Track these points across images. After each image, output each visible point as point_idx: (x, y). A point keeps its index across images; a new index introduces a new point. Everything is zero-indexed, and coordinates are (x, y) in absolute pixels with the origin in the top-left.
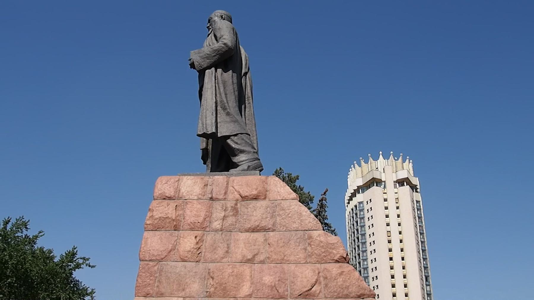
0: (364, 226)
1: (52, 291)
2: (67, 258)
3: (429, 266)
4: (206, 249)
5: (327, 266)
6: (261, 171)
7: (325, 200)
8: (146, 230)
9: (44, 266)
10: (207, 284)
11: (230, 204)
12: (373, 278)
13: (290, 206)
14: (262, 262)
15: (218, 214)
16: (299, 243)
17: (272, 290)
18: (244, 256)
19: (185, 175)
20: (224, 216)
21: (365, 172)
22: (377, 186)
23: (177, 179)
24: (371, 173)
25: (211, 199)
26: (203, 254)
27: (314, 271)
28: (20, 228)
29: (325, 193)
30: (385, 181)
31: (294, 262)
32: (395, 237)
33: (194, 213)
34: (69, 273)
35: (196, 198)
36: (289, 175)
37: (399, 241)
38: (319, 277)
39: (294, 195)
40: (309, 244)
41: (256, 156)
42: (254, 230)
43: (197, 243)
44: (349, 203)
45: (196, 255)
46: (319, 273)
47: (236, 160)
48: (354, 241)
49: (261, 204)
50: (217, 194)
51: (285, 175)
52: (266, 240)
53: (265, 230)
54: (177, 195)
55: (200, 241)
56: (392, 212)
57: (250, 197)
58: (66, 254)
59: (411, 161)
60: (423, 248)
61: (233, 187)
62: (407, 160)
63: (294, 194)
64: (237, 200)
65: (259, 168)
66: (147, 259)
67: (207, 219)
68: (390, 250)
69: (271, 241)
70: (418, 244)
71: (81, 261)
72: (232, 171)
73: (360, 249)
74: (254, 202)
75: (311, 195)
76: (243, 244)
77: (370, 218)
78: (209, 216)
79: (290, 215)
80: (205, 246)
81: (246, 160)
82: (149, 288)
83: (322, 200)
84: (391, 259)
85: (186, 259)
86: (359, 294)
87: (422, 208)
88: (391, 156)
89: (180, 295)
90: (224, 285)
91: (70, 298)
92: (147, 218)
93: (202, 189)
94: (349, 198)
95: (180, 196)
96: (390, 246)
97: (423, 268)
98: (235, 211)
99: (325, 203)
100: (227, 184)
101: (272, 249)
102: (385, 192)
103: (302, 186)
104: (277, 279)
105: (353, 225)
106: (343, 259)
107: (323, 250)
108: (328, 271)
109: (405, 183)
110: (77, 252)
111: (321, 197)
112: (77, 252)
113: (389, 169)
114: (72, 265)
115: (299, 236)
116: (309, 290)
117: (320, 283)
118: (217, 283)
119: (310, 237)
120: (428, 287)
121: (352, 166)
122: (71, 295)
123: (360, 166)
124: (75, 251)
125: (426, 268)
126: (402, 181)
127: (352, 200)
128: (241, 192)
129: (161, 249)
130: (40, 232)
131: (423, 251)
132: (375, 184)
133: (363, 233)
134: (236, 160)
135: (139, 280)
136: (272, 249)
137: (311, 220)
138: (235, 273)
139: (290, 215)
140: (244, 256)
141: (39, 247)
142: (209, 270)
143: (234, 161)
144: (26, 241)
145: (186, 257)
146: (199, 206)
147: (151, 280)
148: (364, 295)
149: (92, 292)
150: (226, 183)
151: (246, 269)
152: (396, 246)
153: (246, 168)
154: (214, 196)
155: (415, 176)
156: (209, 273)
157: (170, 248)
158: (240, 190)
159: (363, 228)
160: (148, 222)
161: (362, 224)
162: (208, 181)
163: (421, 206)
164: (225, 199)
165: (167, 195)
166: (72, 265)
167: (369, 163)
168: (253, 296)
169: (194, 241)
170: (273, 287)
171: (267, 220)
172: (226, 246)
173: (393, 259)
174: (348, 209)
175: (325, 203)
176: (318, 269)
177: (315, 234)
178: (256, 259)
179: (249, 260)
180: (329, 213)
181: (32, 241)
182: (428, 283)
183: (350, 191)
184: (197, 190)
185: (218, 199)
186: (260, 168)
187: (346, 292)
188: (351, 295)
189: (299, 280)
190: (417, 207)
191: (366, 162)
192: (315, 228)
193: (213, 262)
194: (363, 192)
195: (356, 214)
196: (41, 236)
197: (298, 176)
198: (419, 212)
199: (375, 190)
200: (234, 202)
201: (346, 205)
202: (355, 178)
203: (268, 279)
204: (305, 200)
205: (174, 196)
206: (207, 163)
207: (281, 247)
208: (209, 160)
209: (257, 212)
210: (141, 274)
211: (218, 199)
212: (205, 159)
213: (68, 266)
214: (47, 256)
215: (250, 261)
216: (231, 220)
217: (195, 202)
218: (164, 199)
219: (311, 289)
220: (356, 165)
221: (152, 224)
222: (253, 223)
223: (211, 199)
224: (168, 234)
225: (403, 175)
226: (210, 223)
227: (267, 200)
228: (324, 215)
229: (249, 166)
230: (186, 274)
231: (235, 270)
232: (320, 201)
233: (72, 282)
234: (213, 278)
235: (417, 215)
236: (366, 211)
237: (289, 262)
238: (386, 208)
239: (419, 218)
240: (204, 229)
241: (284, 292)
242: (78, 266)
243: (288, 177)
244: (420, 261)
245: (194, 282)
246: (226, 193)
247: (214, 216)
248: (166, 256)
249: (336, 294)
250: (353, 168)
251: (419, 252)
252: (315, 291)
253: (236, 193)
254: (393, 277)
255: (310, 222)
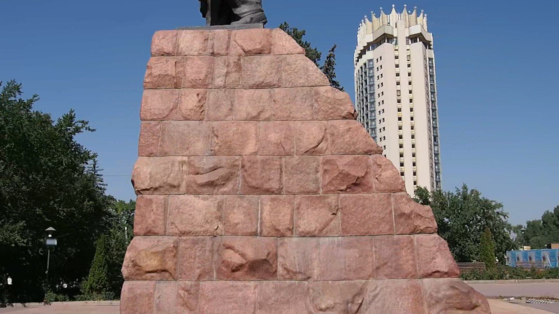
0: (373, 85)
1: (53, 155)
2: (64, 122)
3: (438, 126)
4: (209, 107)
5: (335, 122)
6: (264, 23)
7: (333, 57)
8: (145, 88)
9: (41, 130)
10: (211, 142)
11: (233, 59)
12: (380, 112)
13: (296, 61)
14: (268, 119)
15: (220, 69)
16: (306, 99)
17: (278, 148)
18: (248, 114)
19: (183, 29)
20: (227, 72)
21: (376, 27)
22: (388, 42)
23: (175, 34)
24: (382, 29)
25: (213, 54)
26: (206, 111)
27: (321, 129)
28: (13, 92)
29: (333, 50)
30: (396, 37)
31: (301, 119)
32: (405, 97)
33: (194, 69)
34: (69, 137)
35: (196, 53)
36: (295, 30)
37: (413, 183)
38: (325, 133)
39: (300, 49)
40: (316, 100)
41: (260, 7)
42: (259, 86)
43: (200, 101)
44: (358, 61)
45: (199, 114)
46: (326, 130)
47: (237, 11)
48: (363, 100)
49: (265, 58)
50: (218, 49)
51: (290, 31)
52: (271, 97)
53: (270, 86)
54: (176, 51)
55: (202, 99)
56: (404, 79)
57: (254, 52)
58: (64, 117)
59: (426, 15)
60: (434, 108)
61: (235, 41)
62: (422, 14)
63: (301, 47)
64: (240, 55)
65: (263, 20)
66: (148, 118)
67: (209, 76)
68: (399, 110)
69: (277, 97)
70: (428, 103)
71: (80, 125)
72: (234, 24)
73: (369, 109)
74: (258, 57)
75: (318, 52)
76: (247, 101)
77: (382, 129)
78: (210, 74)
79: (296, 71)
80: (208, 104)
81: (249, 12)
82: (152, 148)
83: (330, 57)
84: (400, 119)
85: (188, 117)
86: (366, 150)
87: (434, 65)
88: (405, 9)
89: (185, 154)
90: (229, 143)
91: (72, 162)
92: (146, 75)
93: (202, 44)
94: (358, 56)
95: (179, 52)
96: (399, 105)
97: (432, 128)
98: (239, 67)
99: (333, 60)
100: (229, 38)
101: (278, 106)
102: (397, 48)
103: (308, 42)
104: (283, 136)
105: (362, 84)
106: (351, 116)
107: (330, 107)
108: (335, 127)
109: (418, 39)
110: (75, 115)
111: (329, 53)
112: (75, 115)
113: (401, 24)
114: (72, 129)
115: (305, 92)
116: (315, 147)
117: (327, 140)
118: (221, 142)
119: (317, 93)
120: (436, 147)
121: (363, 21)
122: (73, 159)
123: (370, 20)
124: (73, 114)
125: (435, 128)
126: (415, 36)
127: (361, 57)
128: (244, 47)
129: (162, 108)
130: (35, 97)
131: (434, 110)
132: (386, 41)
133: (372, 92)
134: (237, 11)
135: (142, 140)
136: (278, 106)
137: (318, 75)
138: (239, 131)
139: (296, 71)
140: (248, 114)
141: (35, 112)
142: (213, 128)
143: (235, 12)
144: (21, 106)
145: (189, 115)
146: (199, 62)
147: (153, 139)
148: (371, 151)
149: (95, 156)
150: (227, 37)
151: (251, 127)
152: (405, 105)
153: (249, 20)
154: (215, 51)
155: (429, 31)
156: (213, 131)
157: (171, 107)
158: (242, 45)
159: (372, 88)
160: (147, 80)
161: (371, 83)
162: (208, 35)
163: (434, 63)
164: (227, 54)
165: (165, 51)
166: (72, 129)
167: (381, 17)
168: (259, 153)
169: (195, 99)
170: (279, 145)
171: (272, 75)
172: (229, 103)
173: (402, 119)
174: (357, 68)
175: (333, 60)
176: (325, 125)
177: (322, 89)
178: (261, 116)
179: (254, 117)
180: (337, 70)
181: (27, 105)
182: (436, 143)
183: (360, 48)
184: (197, 45)
185: (219, 55)
186: (264, 21)
187: (353, 148)
188: (359, 152)
189: (306, 136)
190: (429, 65)
191: (378, 16)
192: (322, 84)
193: (216, 120)
194: (373, 49)
195: (365, 73)
196: (36, 100)
197: (304, 32)
198: (431, 70)
199: (386, 46)
200: (237, 57)
201: (355, 62)
202: (365, 34)
203: (274, 137)
204: (313, 56)
205: (173, 52)
206: (207, 16)
207: (287, 104)
208: (209, 13)
209: (261, 68)
210: (143, 133)
211: (219, 55)
212: (204, 11)
213: (67, 130)
214: (45, 121)
215: (255, 118)
216: (234, 76)
217: (195, 57)
218: (163, 55)
219: (317, 146)
220: (367, 20)
221: (152, 82)
222: (258, 79)
223: (213, 54)
224: (168, 92)
225: (416, 30)
226: (212, 79)
227: (272, 54)
228: (332, 73)
229: (252, 19)
230: (189, 133)
231: (240, 128)
232: (328, 58)
233: (73, 146)
234: (217, 136)
235: (428, 64)
236: (375, 69)
237: (295, 119)
238: (397, 57)
239: (431, 76)
240: (206, 86)
241: (290, 149)
242: (78, 130)
243: (294, 32)
244: (429, 121)
245: (198, 141)
246: (228, 48)
247: (216, 72)
248: (168, 115)
249: (343, 150)
250: (363, 23)
251: (429, 112)
252: (322, 148)
253: (238, 47)
254: (401, 137)
255: (317, 78)
